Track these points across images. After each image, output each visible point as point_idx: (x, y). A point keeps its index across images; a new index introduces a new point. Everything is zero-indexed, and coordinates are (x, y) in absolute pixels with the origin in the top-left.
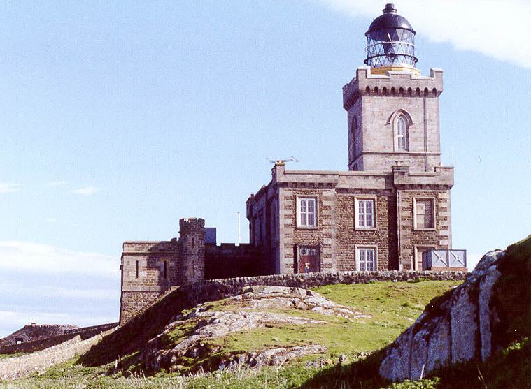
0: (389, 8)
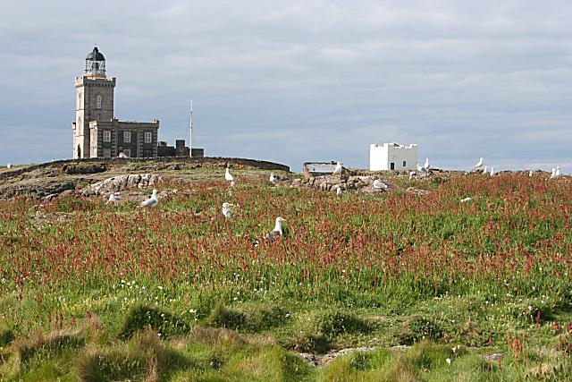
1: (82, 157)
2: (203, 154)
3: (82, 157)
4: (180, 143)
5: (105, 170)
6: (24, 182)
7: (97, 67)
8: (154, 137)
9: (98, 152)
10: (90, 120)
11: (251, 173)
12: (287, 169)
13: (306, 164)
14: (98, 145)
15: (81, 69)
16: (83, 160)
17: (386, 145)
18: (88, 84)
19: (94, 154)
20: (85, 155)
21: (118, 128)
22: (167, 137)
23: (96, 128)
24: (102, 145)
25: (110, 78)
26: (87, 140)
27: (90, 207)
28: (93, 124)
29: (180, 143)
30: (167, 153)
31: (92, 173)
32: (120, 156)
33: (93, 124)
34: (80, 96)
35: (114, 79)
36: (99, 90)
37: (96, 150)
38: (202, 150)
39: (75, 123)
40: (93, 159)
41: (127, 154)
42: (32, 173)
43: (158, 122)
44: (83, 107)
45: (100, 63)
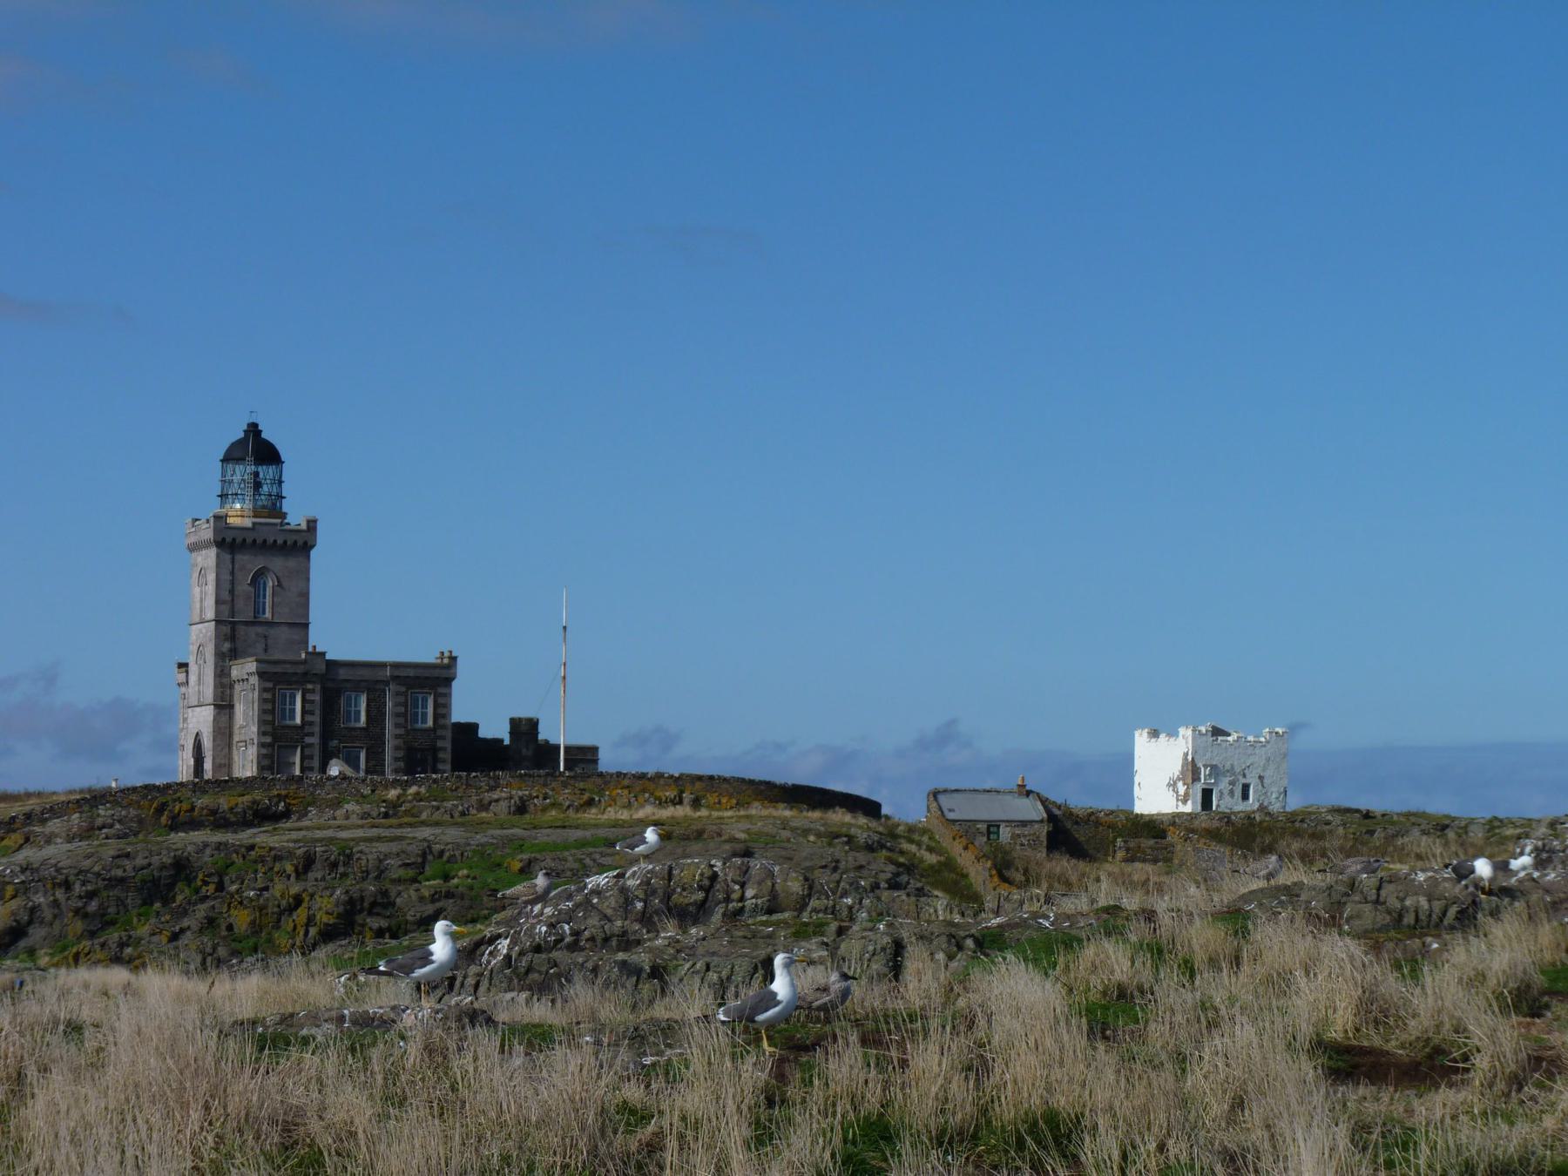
1: (208, 775)
2: (595, 761)
3: (208, 775)
4: (525, 729)
5: (286, 815)
6: (28, 854)
7: (257, 486)
8: (442, 709)
9: (260, 757)
10: (234, 654)
11: (739, 821)
12: (870, 808)
13: (935, 794)
14: (262, 733)
15: (201, 493)
16: (217, 783)
17: (1186, 733)
18: (229, 542)
19: (245, 765)
20: (216, 767)
21: (334, 682)
22: (484, 706)
23: (254, 680)
24: (278, 739)
25: (296, 516)
26: (224, 718)
27: (502, 1051)
28: (245, 669)
29: (525, 729)
30: (472, 752)
31: (247, 824)
32: (334, 771)
33: (245, 669)
34: (202, 581)
35: (312, 525)
36: (263, 556)
37: (252, 752)
38: (594, 750)
39: (183, 666)
40: (247, 783)
41: (352, 762)
42: (54, 825)
43: (453, 659)
44: (210, 614)
45: (266, 472)
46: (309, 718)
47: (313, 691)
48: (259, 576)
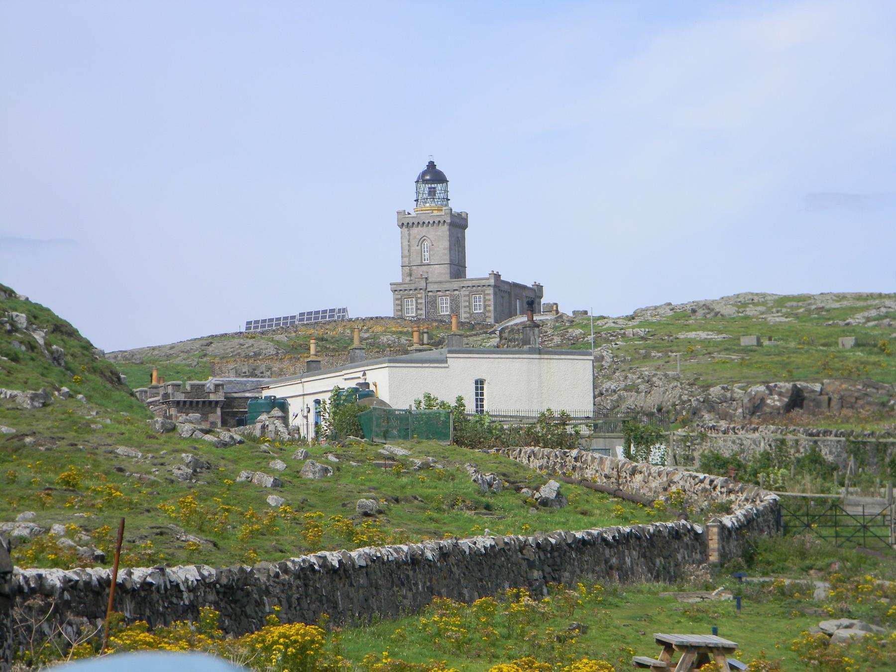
0: (432, 165)
46: (419, 312)
47: (421, 298)
48: (422, 240)
